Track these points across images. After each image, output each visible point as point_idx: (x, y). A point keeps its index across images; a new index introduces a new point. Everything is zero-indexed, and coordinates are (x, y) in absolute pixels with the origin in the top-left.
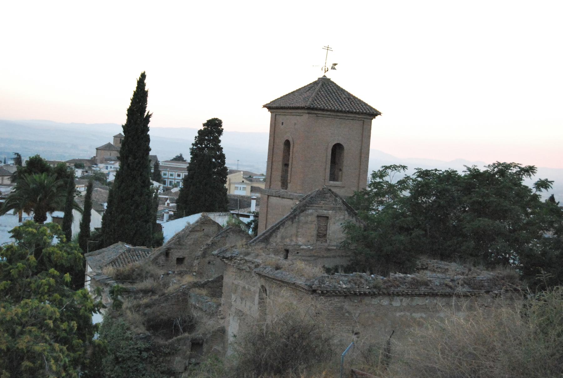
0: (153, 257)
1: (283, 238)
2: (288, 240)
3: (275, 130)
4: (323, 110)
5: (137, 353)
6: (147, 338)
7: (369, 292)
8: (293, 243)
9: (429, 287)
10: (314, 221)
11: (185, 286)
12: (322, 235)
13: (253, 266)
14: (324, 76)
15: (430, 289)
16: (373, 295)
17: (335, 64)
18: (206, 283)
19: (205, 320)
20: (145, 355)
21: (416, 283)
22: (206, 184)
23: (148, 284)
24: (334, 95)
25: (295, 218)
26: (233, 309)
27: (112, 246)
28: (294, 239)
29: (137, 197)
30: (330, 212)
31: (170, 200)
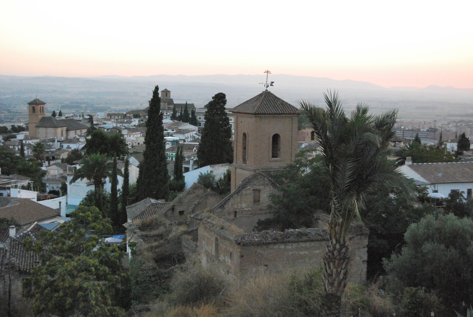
0: (164, 212)
1: (232, 205)
2: (236, 206)
3: (237, 126)
5: (148, 278)
6: (154, 269)
7: (271, 242)
8: (239, 207)
9: (308, 237)
10: (251, 193)
11: (179, 234)
12: (257, 201)
13: (211, 225)
14: (266, 90)
15: (308, 237)
16: (275, 243)
17: (273, 82)
19: (190, 254)
20: (153, 279)
24: (272, 102)
25: (240, 192)
26: (203, 250)
27: (143, 201)
28: (239, 205)
29: (157, 168)
30: (261, 187)
31: (196, 148)
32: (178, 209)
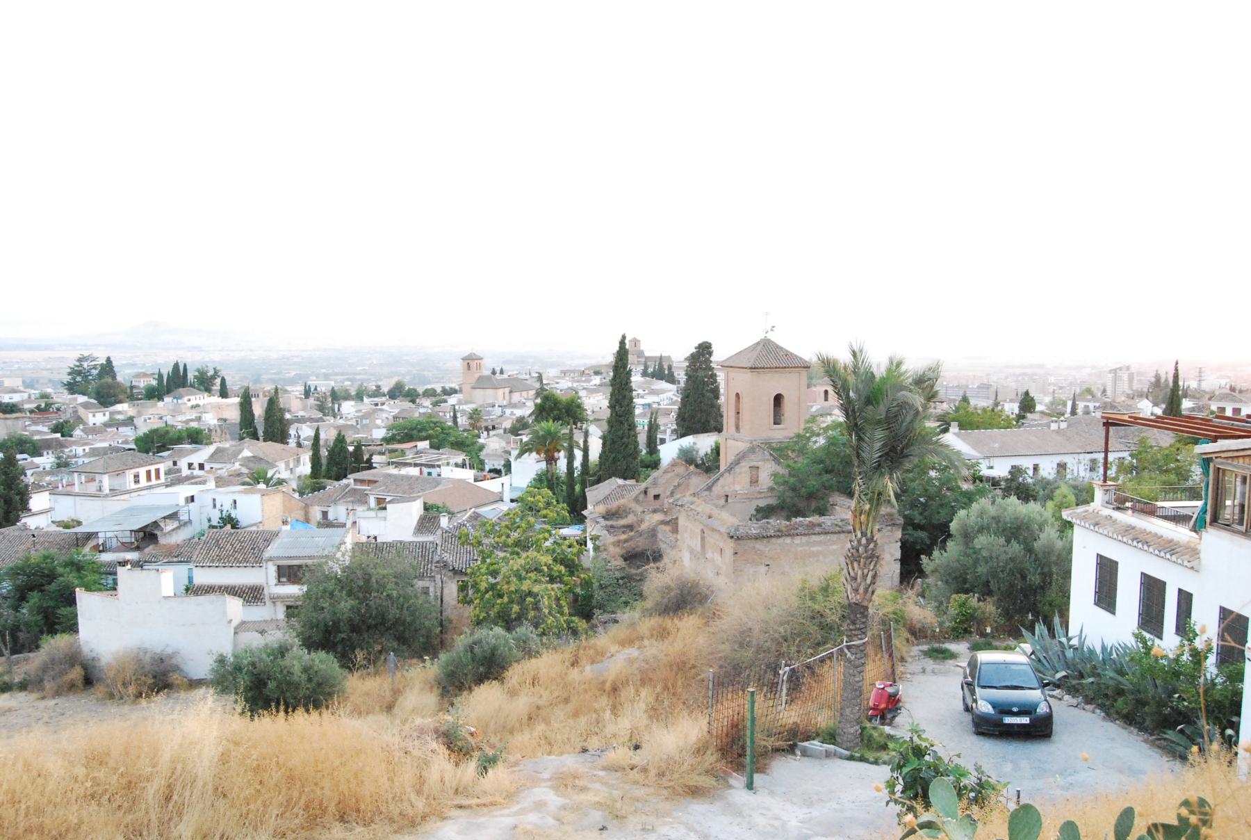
0: (634, 495)
1: (723, 487)
2: (727, 488)
4: (763, 368)
6: (623, 569)
12: (754, 481)
16: (779, 537)
18: (670, 521)
19: (668, 551)
21: (813, 525)
22: (701, 402)
23: (630, 519)
27: (607, 482)
28: (732, 486)
29: (625, 440)
30: (760, 463)
32: (652, 492)
